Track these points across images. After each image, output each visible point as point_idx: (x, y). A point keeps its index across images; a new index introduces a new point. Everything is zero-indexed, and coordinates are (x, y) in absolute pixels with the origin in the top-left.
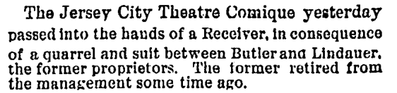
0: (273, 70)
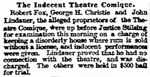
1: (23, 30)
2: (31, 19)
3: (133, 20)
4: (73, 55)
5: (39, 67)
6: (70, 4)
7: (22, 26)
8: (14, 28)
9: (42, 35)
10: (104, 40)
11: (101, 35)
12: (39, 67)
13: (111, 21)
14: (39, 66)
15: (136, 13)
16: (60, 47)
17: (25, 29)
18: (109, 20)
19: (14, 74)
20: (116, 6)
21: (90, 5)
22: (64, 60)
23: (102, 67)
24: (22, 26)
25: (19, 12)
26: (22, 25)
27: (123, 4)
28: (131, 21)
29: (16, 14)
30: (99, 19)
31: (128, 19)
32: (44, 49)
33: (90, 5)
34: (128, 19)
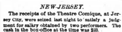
0: (31, 20)
1: (82, 15)
2: (118, 13)
3: (57, 14)
4: (117, 15)
5: (114, 27)
6: (9, 13)
7: (81, 12)
8: (75, 14)
9: (69, 14)
10: (73, 13)
11: (42, 14)
12: (59, 15)
13: (42, 14)
14: (114, 26)
15: (115, 14)
16: (104, 14)
17: (83, 14)
18: (40, 14)
19: (110, 13)
20: (89, 15)
21: (71, 14)
22: (49, 14)
23: (26, 14)
24: (81, 12)
25: (43, 25)
26: (81, 11)
27: (94, 13)
28: (56, 14)
29: (80, 20)
30: (79, 19)
31: (15, 13)
32: (27, 15)
33: (71, 14)
34: (15, 13)
